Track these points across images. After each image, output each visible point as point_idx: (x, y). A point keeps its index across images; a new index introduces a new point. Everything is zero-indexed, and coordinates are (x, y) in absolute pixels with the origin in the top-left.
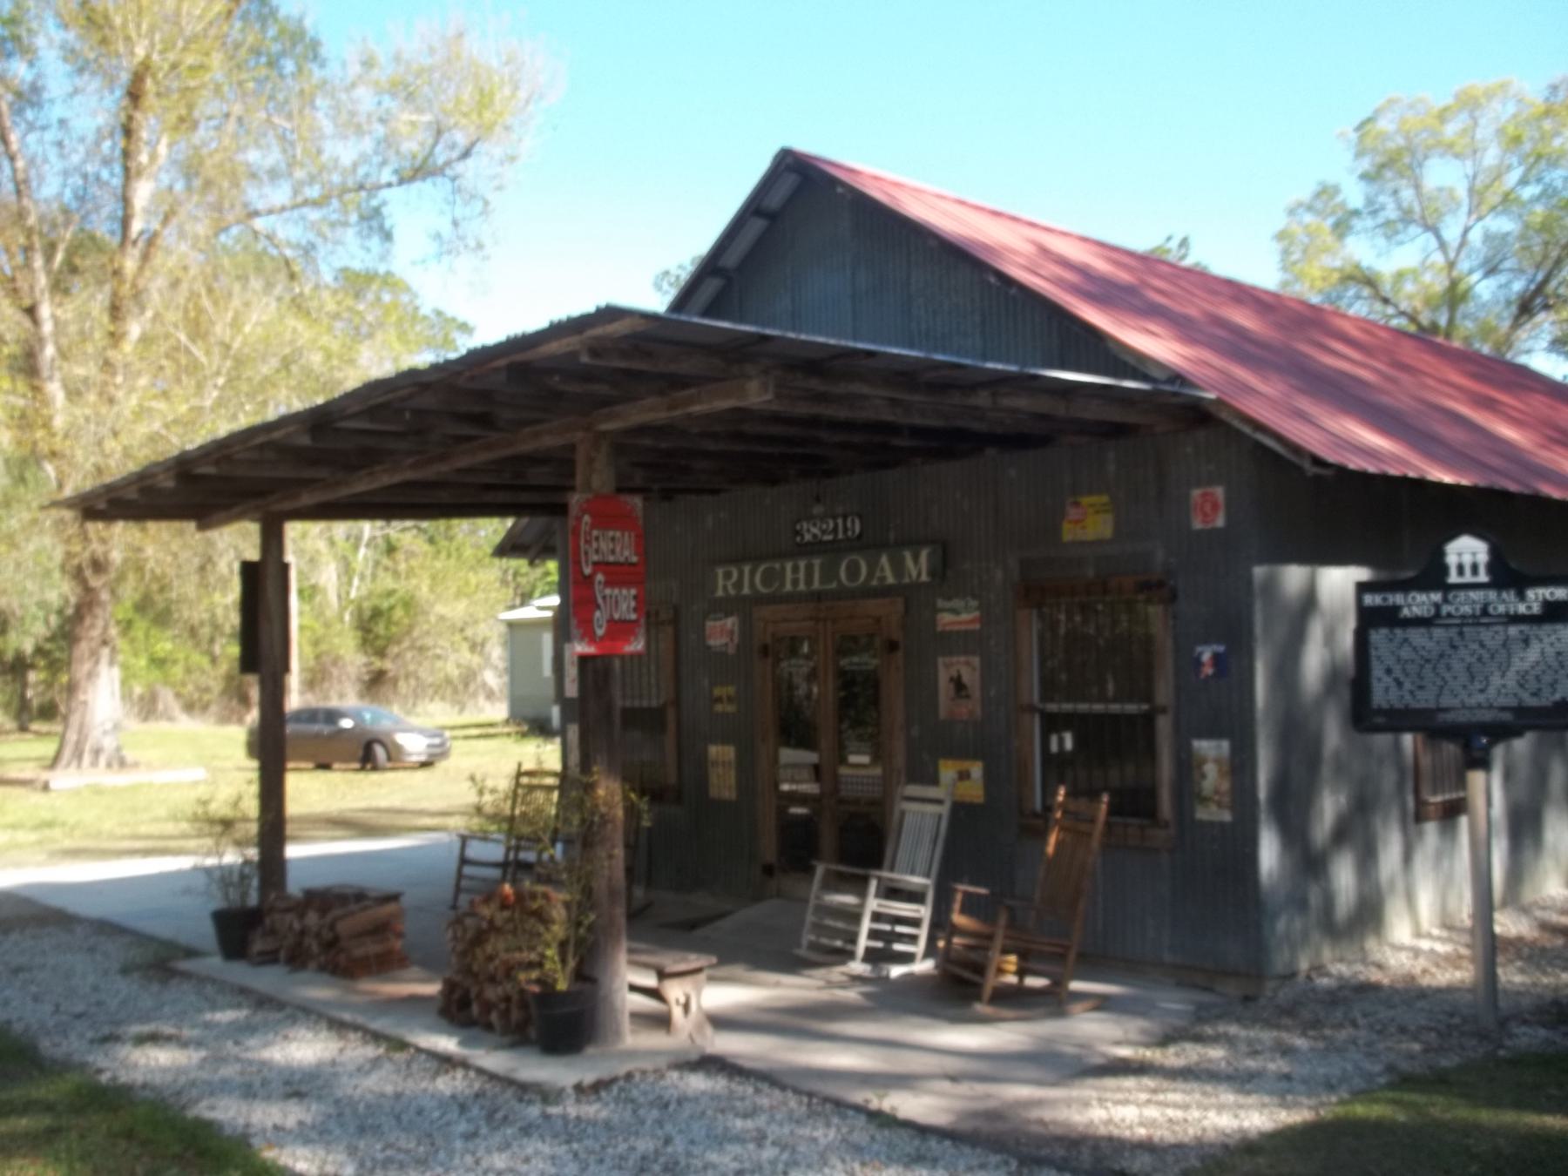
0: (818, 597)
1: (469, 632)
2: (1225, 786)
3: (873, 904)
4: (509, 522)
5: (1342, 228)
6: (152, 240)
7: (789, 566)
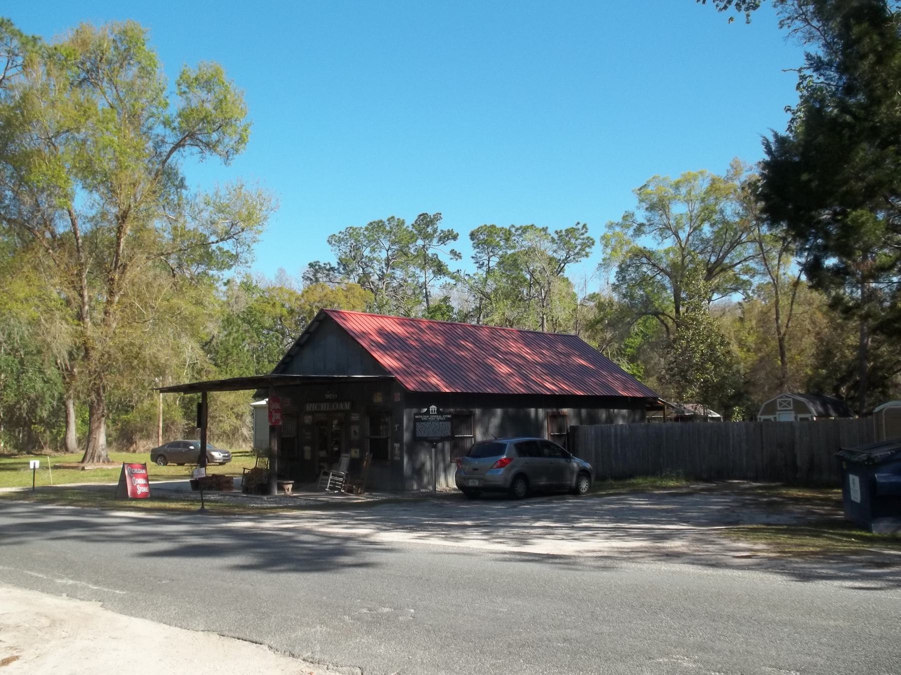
1: (236, 410)
3: (331, 477)
5: (639, 230)
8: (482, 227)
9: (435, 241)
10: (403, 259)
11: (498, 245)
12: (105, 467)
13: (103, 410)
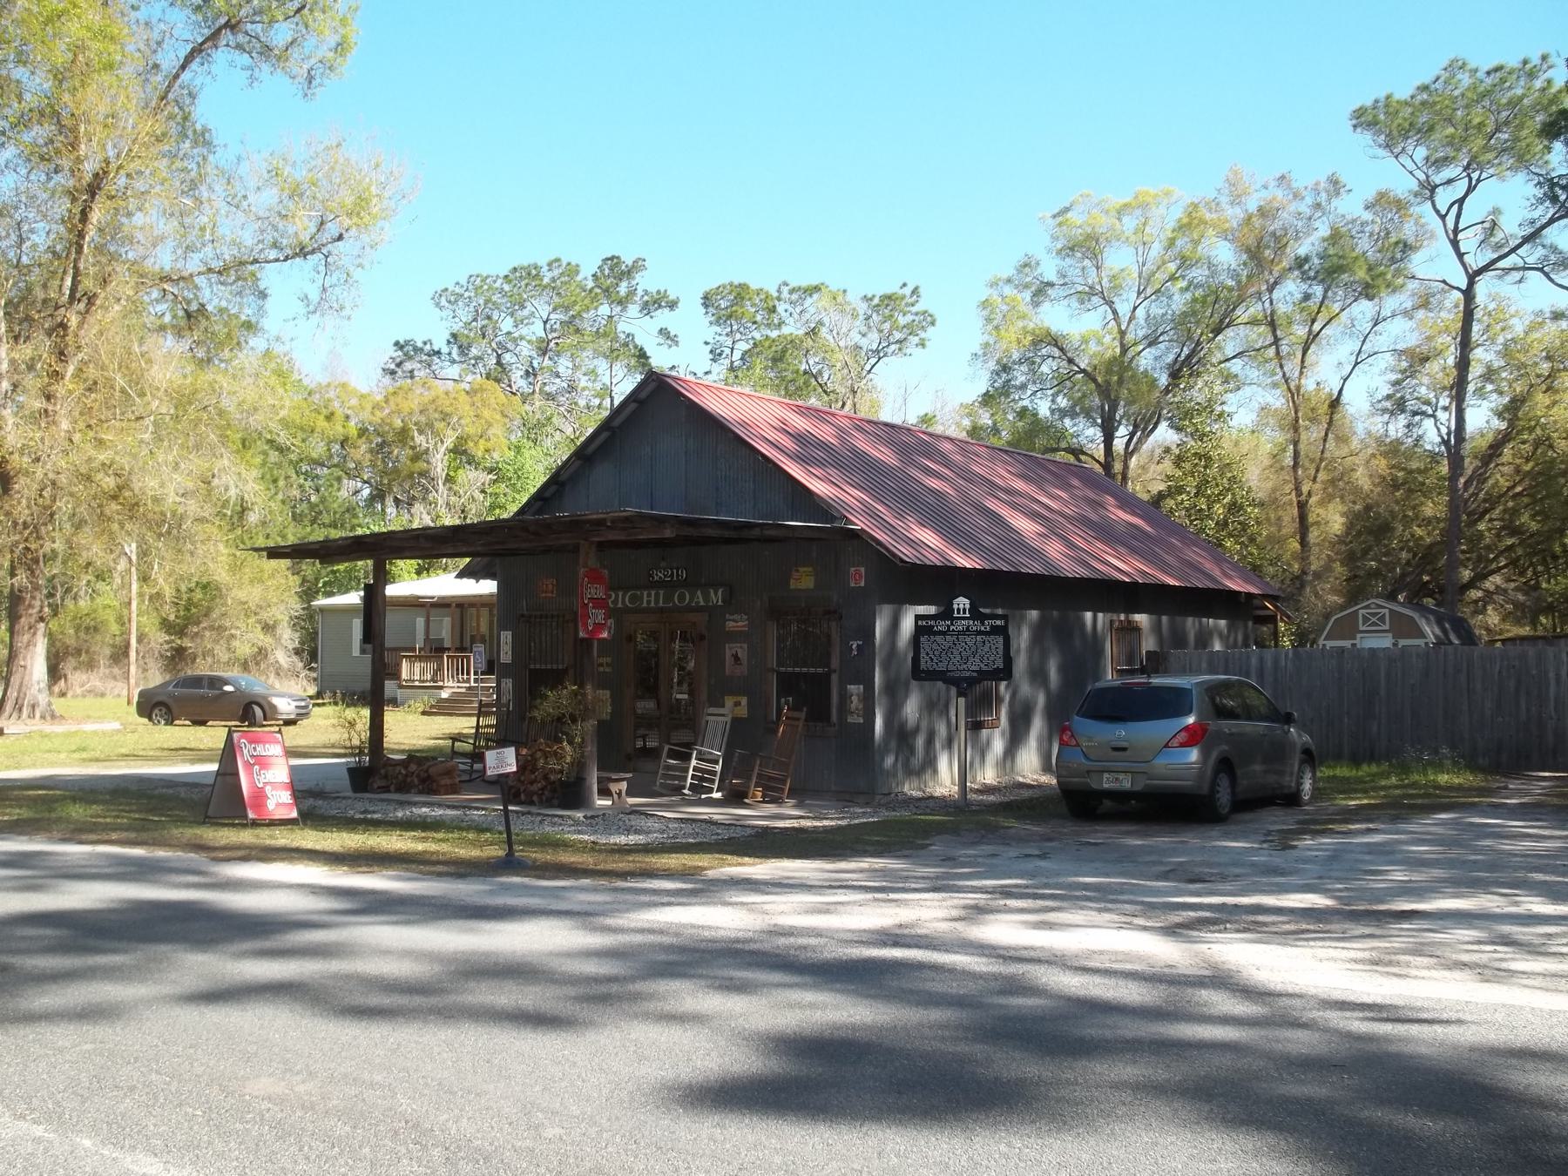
0: (662, 610)
1: (264, 615)
2: (861, 707)
3: (694, 762)
4: (468, 560)
5: (1041, 291)
7: (645, 593)
8: (724, 287)
9: (633, 310)
10: (574, 339)
12: (48, 728)
13: (42, 607)
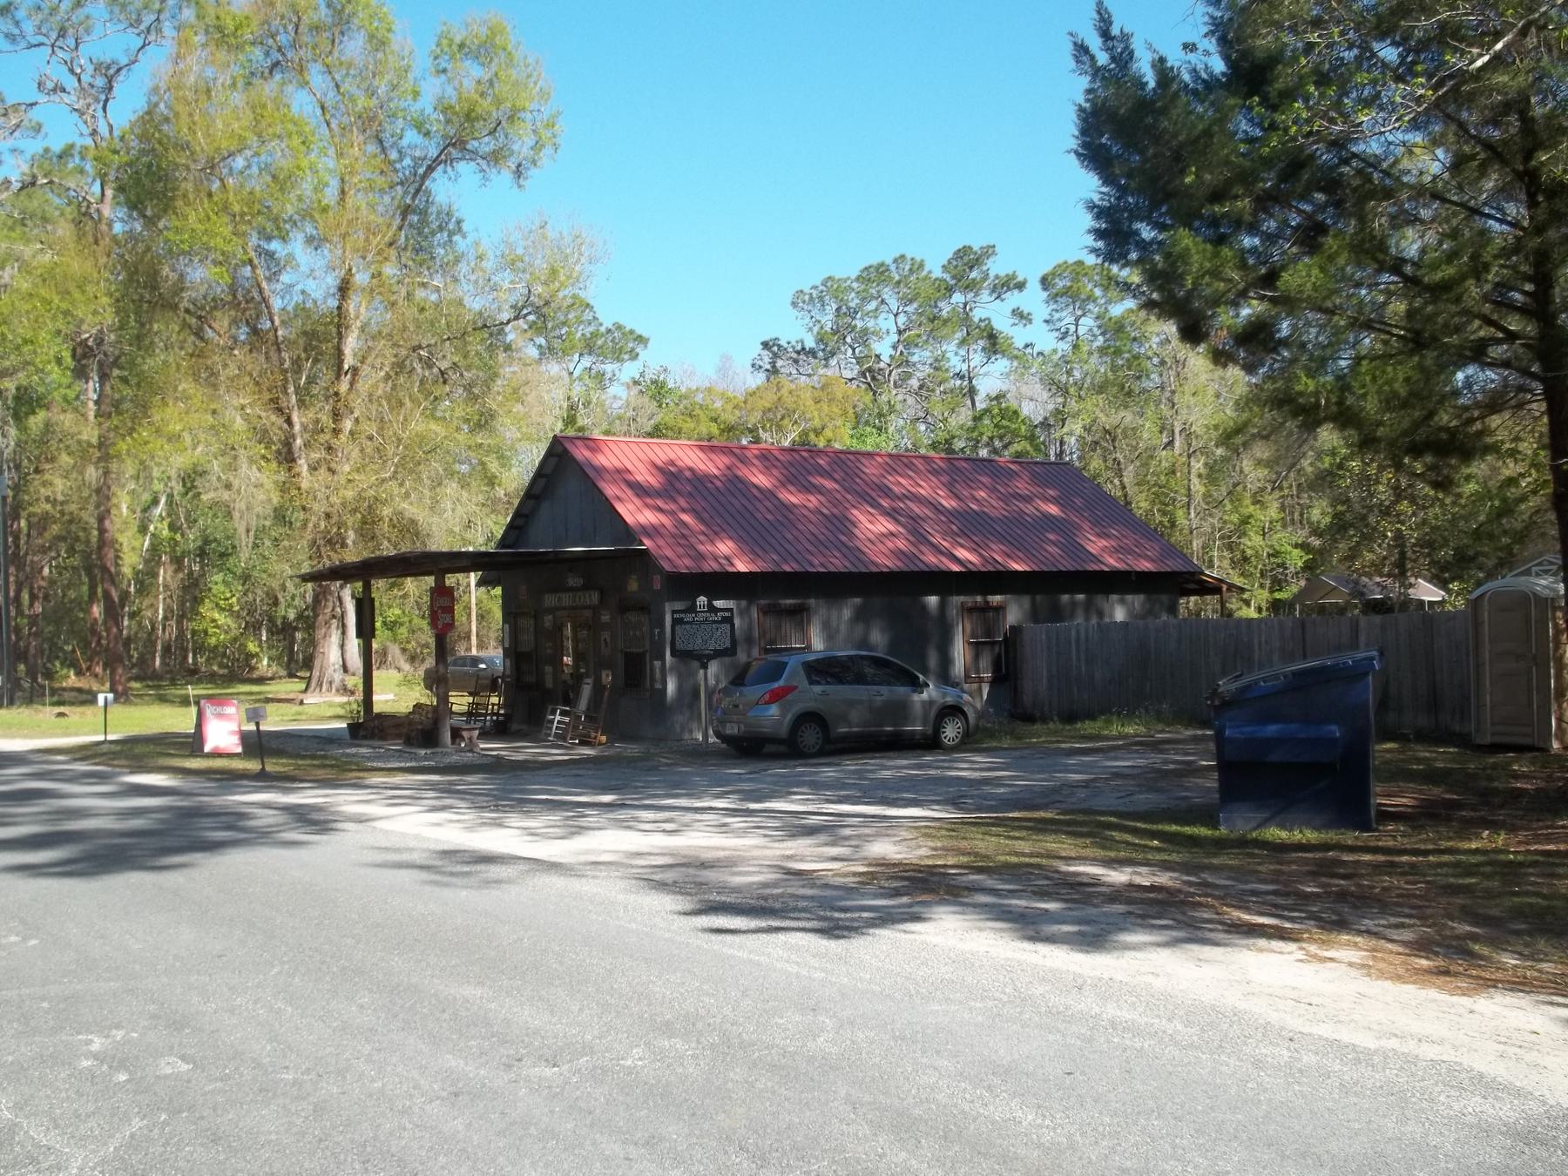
3: (558, 718)
6: (355, 371)
8: (1059, 266)
9: (985, 296)
11: (1090, 298)
